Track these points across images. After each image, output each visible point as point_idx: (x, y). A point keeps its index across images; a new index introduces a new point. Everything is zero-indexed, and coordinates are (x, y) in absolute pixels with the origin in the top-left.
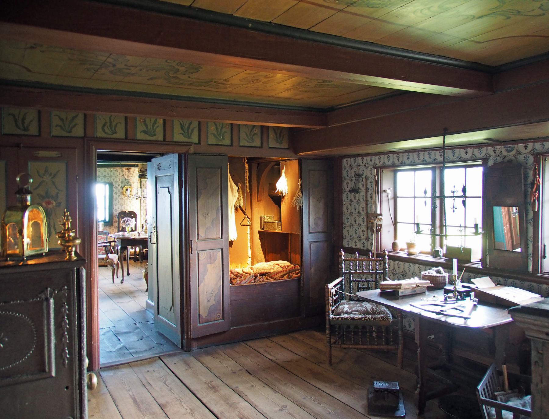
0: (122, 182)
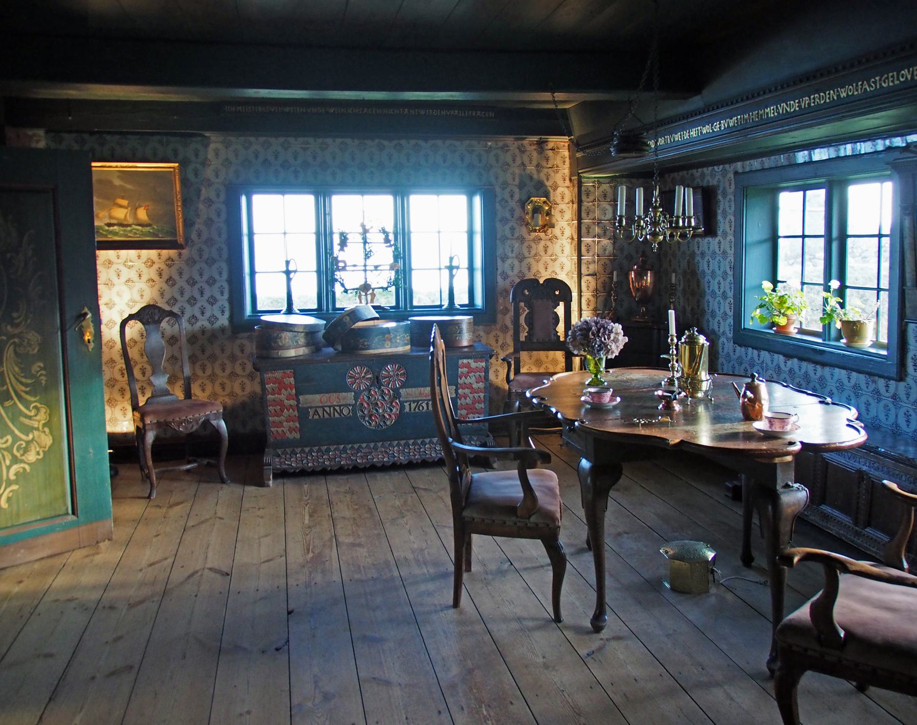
0: (521, 186)
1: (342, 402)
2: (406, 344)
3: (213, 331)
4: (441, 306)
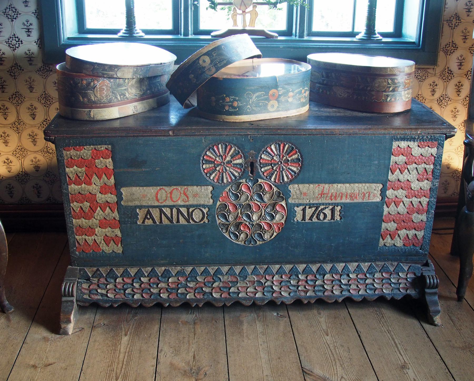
1: (192, 201)
2: (303, 105)
3: (15, 58)
4: (352, 34)
